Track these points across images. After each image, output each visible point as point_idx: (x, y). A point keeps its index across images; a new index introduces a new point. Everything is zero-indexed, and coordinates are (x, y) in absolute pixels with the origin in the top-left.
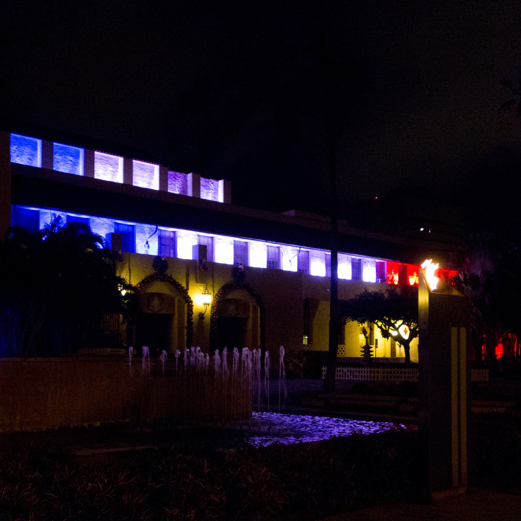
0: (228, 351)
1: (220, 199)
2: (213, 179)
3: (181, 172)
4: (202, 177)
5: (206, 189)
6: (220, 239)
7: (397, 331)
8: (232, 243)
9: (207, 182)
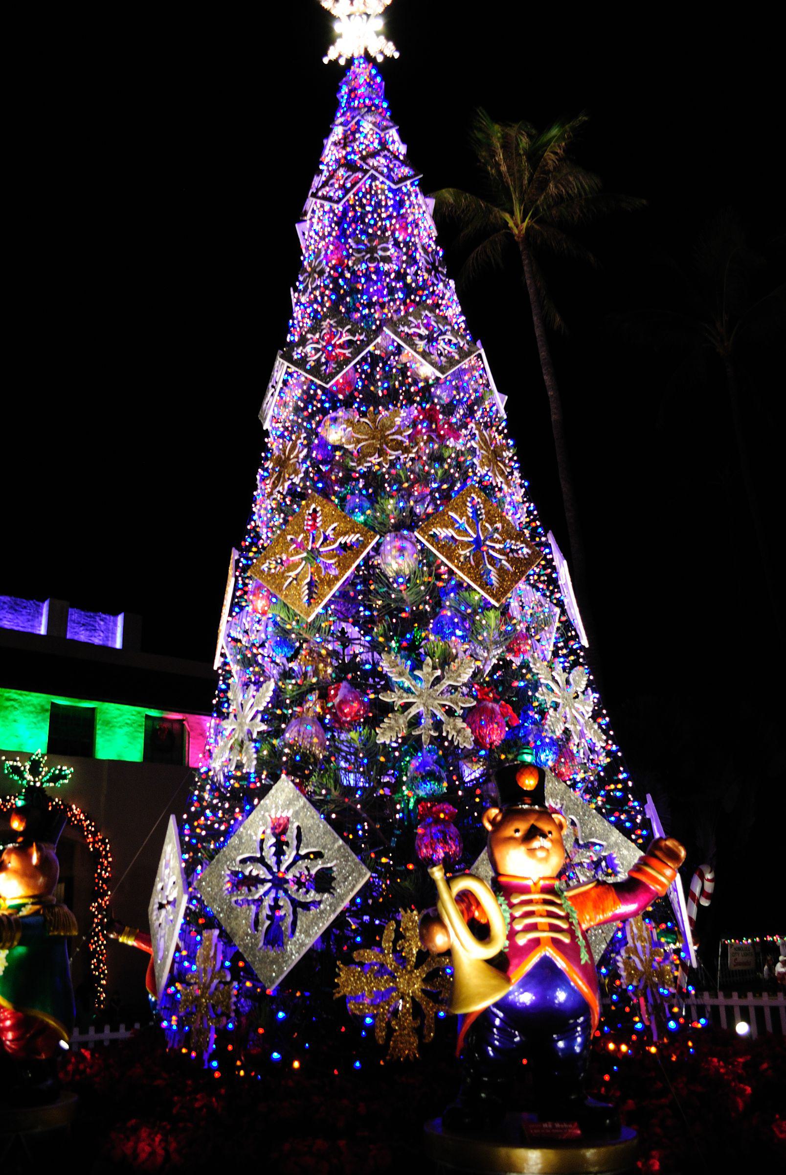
0: (181, 983)
1: (43, 631)
2: (105, 614)
3: (29, 597)
4: (72, 607)
5: (87, 630)
6: (11, 700)
7: (443, 931)
8: (47, 710)
9: (90, 617)
